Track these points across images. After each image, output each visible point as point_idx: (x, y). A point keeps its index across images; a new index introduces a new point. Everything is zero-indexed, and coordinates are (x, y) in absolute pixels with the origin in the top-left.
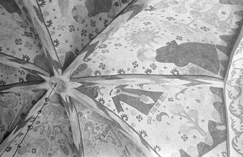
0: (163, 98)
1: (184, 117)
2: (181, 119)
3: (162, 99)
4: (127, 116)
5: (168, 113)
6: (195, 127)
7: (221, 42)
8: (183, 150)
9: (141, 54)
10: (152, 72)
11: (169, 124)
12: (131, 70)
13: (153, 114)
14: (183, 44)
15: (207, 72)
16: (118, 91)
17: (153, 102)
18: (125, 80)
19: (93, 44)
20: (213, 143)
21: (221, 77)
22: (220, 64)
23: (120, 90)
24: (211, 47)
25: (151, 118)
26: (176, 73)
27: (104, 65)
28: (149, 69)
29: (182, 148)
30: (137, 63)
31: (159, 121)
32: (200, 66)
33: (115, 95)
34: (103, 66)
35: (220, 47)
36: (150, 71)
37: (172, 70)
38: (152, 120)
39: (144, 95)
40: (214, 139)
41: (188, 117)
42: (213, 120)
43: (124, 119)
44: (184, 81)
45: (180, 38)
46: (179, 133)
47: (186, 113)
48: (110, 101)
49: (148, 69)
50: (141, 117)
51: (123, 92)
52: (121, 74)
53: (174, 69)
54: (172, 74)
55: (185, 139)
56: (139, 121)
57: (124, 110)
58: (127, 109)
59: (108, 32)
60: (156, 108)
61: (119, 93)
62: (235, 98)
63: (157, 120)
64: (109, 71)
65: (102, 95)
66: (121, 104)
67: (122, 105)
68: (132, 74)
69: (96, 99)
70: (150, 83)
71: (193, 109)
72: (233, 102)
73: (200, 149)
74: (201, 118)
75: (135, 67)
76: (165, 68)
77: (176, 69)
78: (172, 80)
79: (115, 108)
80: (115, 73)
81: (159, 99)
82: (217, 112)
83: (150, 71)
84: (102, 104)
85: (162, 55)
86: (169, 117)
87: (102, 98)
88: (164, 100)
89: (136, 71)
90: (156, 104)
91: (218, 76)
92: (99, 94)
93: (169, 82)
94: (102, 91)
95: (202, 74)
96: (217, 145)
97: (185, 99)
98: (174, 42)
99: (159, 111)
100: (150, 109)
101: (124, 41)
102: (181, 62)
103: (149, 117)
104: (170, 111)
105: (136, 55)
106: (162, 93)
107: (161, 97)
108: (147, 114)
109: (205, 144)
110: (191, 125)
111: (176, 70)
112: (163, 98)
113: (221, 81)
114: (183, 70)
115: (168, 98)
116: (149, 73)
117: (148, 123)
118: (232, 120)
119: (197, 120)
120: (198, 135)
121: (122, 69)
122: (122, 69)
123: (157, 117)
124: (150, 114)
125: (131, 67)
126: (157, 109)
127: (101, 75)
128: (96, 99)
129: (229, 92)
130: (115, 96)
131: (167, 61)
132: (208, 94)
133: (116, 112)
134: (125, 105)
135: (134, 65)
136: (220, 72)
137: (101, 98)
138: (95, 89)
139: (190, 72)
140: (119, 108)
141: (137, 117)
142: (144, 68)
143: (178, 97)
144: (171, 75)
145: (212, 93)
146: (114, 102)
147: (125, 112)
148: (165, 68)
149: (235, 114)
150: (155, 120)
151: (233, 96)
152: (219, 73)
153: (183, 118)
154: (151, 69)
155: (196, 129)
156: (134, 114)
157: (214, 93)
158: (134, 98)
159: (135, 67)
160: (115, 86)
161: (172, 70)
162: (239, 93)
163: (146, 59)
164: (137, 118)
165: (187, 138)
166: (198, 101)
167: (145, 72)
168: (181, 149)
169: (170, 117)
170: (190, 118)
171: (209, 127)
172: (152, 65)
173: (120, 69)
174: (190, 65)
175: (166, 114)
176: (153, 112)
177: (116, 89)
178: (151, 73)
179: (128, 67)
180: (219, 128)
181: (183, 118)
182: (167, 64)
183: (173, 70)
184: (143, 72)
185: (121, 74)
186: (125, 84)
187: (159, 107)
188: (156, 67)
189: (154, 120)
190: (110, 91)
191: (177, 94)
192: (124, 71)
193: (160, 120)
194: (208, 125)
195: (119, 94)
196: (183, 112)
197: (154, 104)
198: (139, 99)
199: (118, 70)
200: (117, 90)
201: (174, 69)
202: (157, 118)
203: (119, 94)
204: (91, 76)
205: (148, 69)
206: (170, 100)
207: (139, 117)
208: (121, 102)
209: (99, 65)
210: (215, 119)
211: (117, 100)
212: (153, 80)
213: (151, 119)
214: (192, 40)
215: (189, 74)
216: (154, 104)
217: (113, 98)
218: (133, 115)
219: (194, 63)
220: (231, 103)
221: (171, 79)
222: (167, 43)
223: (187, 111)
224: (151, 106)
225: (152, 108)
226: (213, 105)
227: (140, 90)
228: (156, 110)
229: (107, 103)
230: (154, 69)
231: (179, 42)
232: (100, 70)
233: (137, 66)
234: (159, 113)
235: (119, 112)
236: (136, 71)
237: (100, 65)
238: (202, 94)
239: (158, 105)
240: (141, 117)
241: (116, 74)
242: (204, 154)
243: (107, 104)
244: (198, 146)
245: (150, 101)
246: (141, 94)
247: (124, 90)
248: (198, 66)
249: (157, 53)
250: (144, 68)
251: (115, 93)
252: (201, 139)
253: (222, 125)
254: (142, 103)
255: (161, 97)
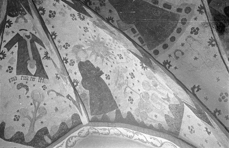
0: (42, 81)
1: (35, 106)
2: (31, 104)
3: (41, 80)
4: (5, 58)
5: (30, 91)
6: (32, 120)
7: (124, 113)
8: (5, 124)
9: (80, 48)
10: (66, 64)
11: (20, 98)
12: (60, 44)
13: (21, 79)
14: (103, 81)
15: (88, 107)
16: (28, 37)
17: (33, 74)
18: (49, 44)
19: (85, 11)
20: (29, 141)
21: (91, 119)
22: (102, 115)
23: (31, 38)
24: (114, 105)
25: (16, 80)
26: (75, 84)
27: (54, 16)
28: (68, 60)
29: (6, 123)
30: (68, 48)
31: (17, 88)
32: (91, 100)
33: (22, 35)
34: (52, 15)
35: (118, 112)
36: (67, 62)
37: (76, 80)
38: (14, 81)
39: (37, 63)
40: (34, 140)
41: (37, 108)
42: (49, 130)
43: (167, 65)
44: (74, 95)
45: (108, 77)
46: (18, 111)
47: (39, 106)
48: (13, 32)
49: (67, 59)
50: (11, 70)
51: (29, 42)
52: (51, 36)
53: (78, 81)
54: (73, 82)
55: (16, 119)
56: (7, 71)
57: (10, 51)
58: (12, 53)
59: (108, 28)
60: (29, 79)
61: (27, 38)
62: (79, 136)
63: (17, 86)
64: (49, 23)
65: (16, 22)
66: (15, 45)
67: (14, 46)
68: (56, 47)
69: (8, 16)
70: (58, 68)
71: (47, 109)
72: (75, 137)
73: (16, 136)
74: (43, 119)
75: (64, 46)
76: (75, 73)
77: (78, 82)
78: (70, 85)
79: (7, 41)
80: (50, 30)
81: (40, 77)
82: (58, 129)
83: (67, 62)
84: (6, 26)
85: (85, 66)
86: (26, 94)
87: (12, 23)
88: (40, 82)
89: (60, 49)
90: (33, 77)
91: (91, 117)
92: (15, 18)
93: (67, 84)
94: (21, 20)
95: (85, 104)
96: (29, 146)
97: (52, 98)
98: (102, 73)
99: (27, 83)
100: (24, 74)
101: (93, 35)
102: (86, 83)
103: (16, 77)
104: (33, 91)
105: (77, 44)
106: (47, 78)
107: (43, 78)
108: (18, 73)
109: (23, 137)
110: (31, 116)
111: (77, 83)
112: (42, 81)
113: (88, 121)
114: (80, 88)
115: (45, 85)
116: (64, 61)
117: (9, 80)
118: (62, 145)
119: (39, 117)
120: (27, 126)
121: (57, 36)
122: (57, 36)
123: (20, 84)
124: (19, 77)
125: (63, 43)
126: (28, 80)
127: (42, 16)
128: (8, 16)
129: (83, 130)
130: (21, 35)
131: (82, 72)
132: (68, 114)
133: (4, 44)
134: (15, 49)
135: (66, 45)
136: (95, 117)
137: (12, 23)
138: (21, 12)
139: (81, 94)
140: (9, 46)
141: (9, 67)
142: (67, 55)
143: (51, 92)
144: (72, 81)
145: (71, 117)
146: (14, 37)
147: (8, 53)
148: (75, 73)
149: (68, 142)
150: (16, 84)
151: (80, 134)
152: (92, 116)
153: (33, 105)
154: (69, 62)
155: (31, 121)
156: (11, 62)
157: (72, 118)
158: (28, 55)
159: (64, 46)
160: (33, 32)
161: (76, 80)
162: (84, 136)
163: (77, 55)
164: (8, 68)
165: (18, 120)
166: (56, 109)
167: (64, 58)
168: (5, 123)
169: (27, 95)
170: (36, 111)
171: (40, 131)
172: (72, 61)
173: (56, 33)
174: (87, 92)
175: (27, 90)
176: (23, 78)
177: (29, 34)
178: (65, 64)
179: (61, 39)
180: (46, 138)
181: (33, 105)
182: (79, 74)
183: (77, 80)
184: (63, 56)
185: (52, 36)
186: (45, 45)
187: (31, 80)
188: (73, 66)
189: (15, 83)
190: (26, 29)
191: (53, 91)
192: (56, 38)
193: (19, 89)
194: (41, 129)
195: (26, 39)
196: (38, 103)
197: (31, 75)
198: (29, 59)
199: (54, 32)
200: (28, 35)
201: (78, 81)
202: (18, 85)
203: (26, 39)
204: (36, 4)
205: (67, 59)
206: (44, 87)
207: (10, 69)
208: (17, 44)
209: (53, 10)
210: (51, 130)
211: (18, 39)
212: (62, 70)
213: (15, 80)
214: (111, 88)
215: (79, 94)
216: (31, 75)
217: (18, 34)
218: (9, 62)
219: (90, 94)
220: (74, 136)
221: (70, 84)
222: (98, 67)
223: (42, 105)
224: (28, 73)
225: (26, 76)
226: (61, 123)
227: (40, 57)
228: (26, 79)
229: (9, 31)
230: (70, 65)
231: (103, 77)
232: (47, 13)
233: (66, 48)
234: (25, 84)
235: (5, 47)
236: (60, 49)
237: (53, 11)
238: (65, 110)
239: (33, 80)
240: (11, 70)
241: (50, 32)
242: (14, 142)
243: (8, 31)
244: (17, 133)
245: (33, 71)
246: (35, 60)
247: (32, 42)
248: (89, 98)
249: (85, 62)
250: (67, 55)
251: (24, 34)
252: (25, 131)
253: (50, 138)
254: (27, 64)
255: (43, 78)
